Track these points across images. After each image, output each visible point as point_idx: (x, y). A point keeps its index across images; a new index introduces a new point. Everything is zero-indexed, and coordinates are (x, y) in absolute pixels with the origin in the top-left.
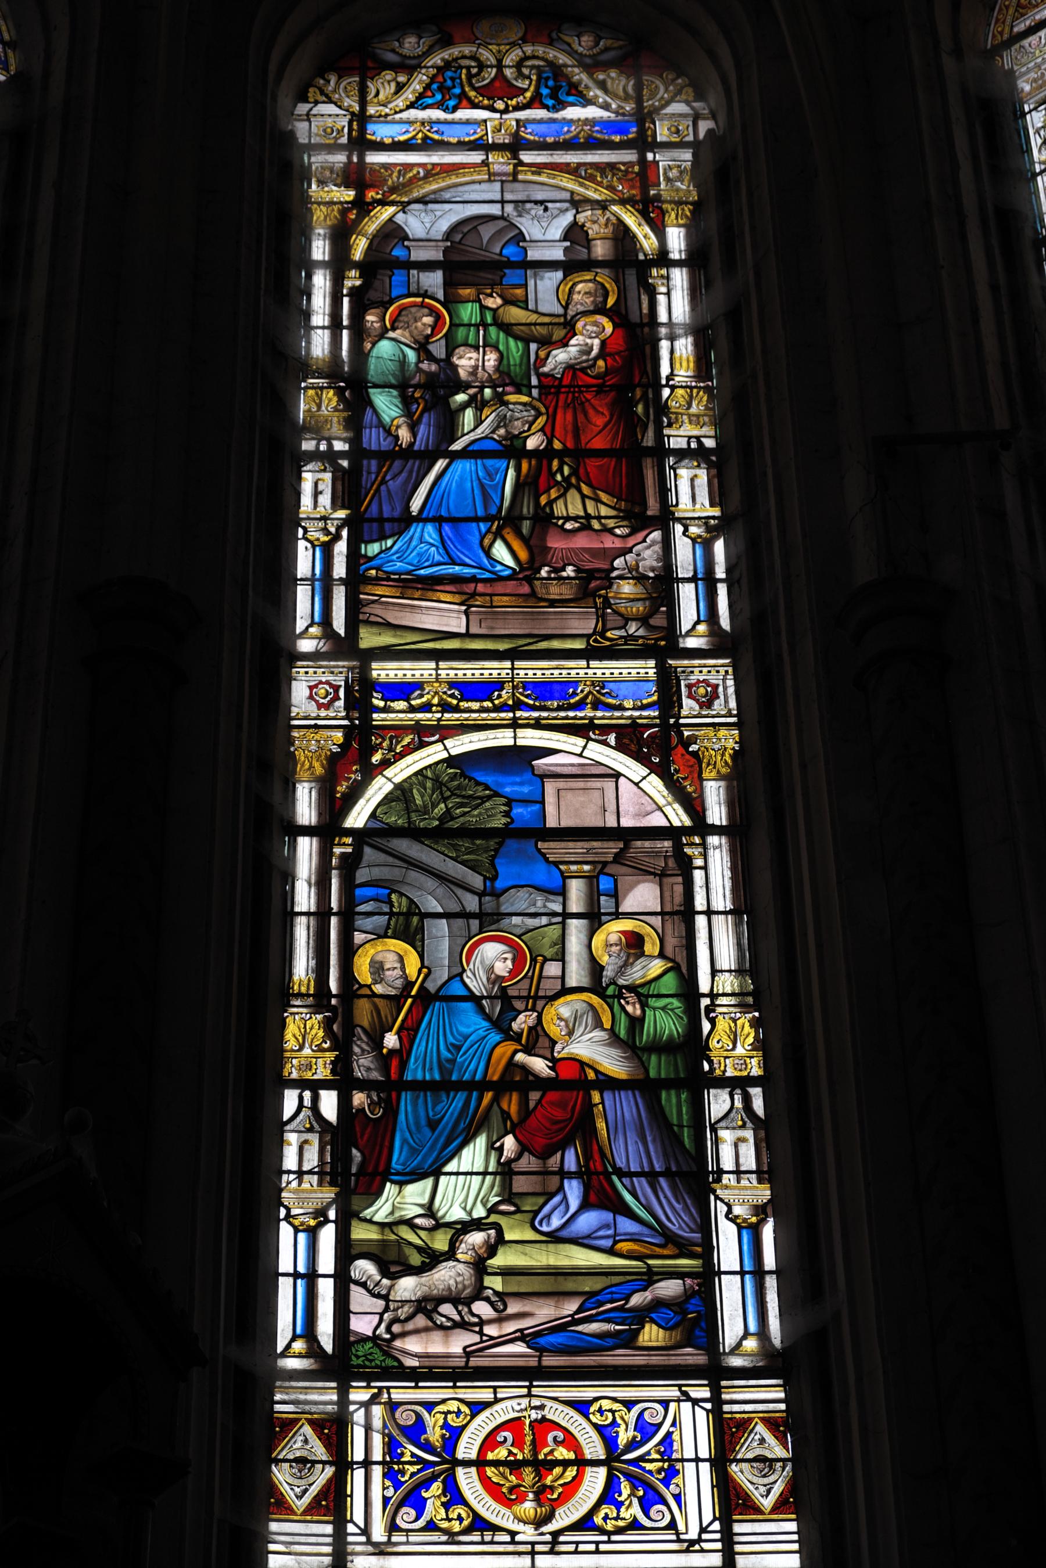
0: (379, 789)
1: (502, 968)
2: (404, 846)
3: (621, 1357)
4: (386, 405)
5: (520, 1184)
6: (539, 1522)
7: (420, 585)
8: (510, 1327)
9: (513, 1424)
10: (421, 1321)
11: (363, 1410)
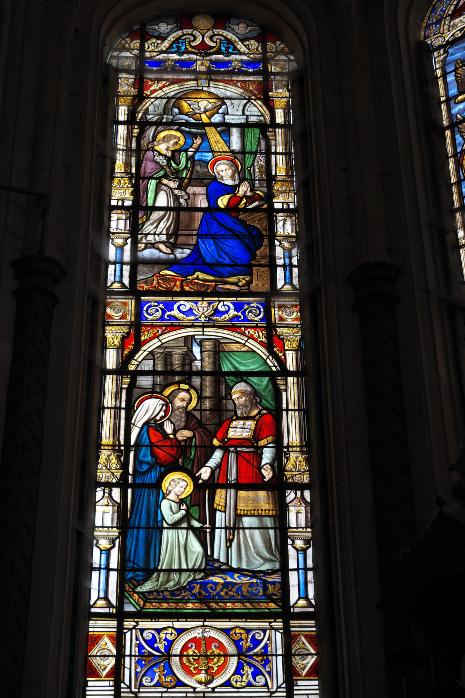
6: (206, 684)
11: (130, 632)
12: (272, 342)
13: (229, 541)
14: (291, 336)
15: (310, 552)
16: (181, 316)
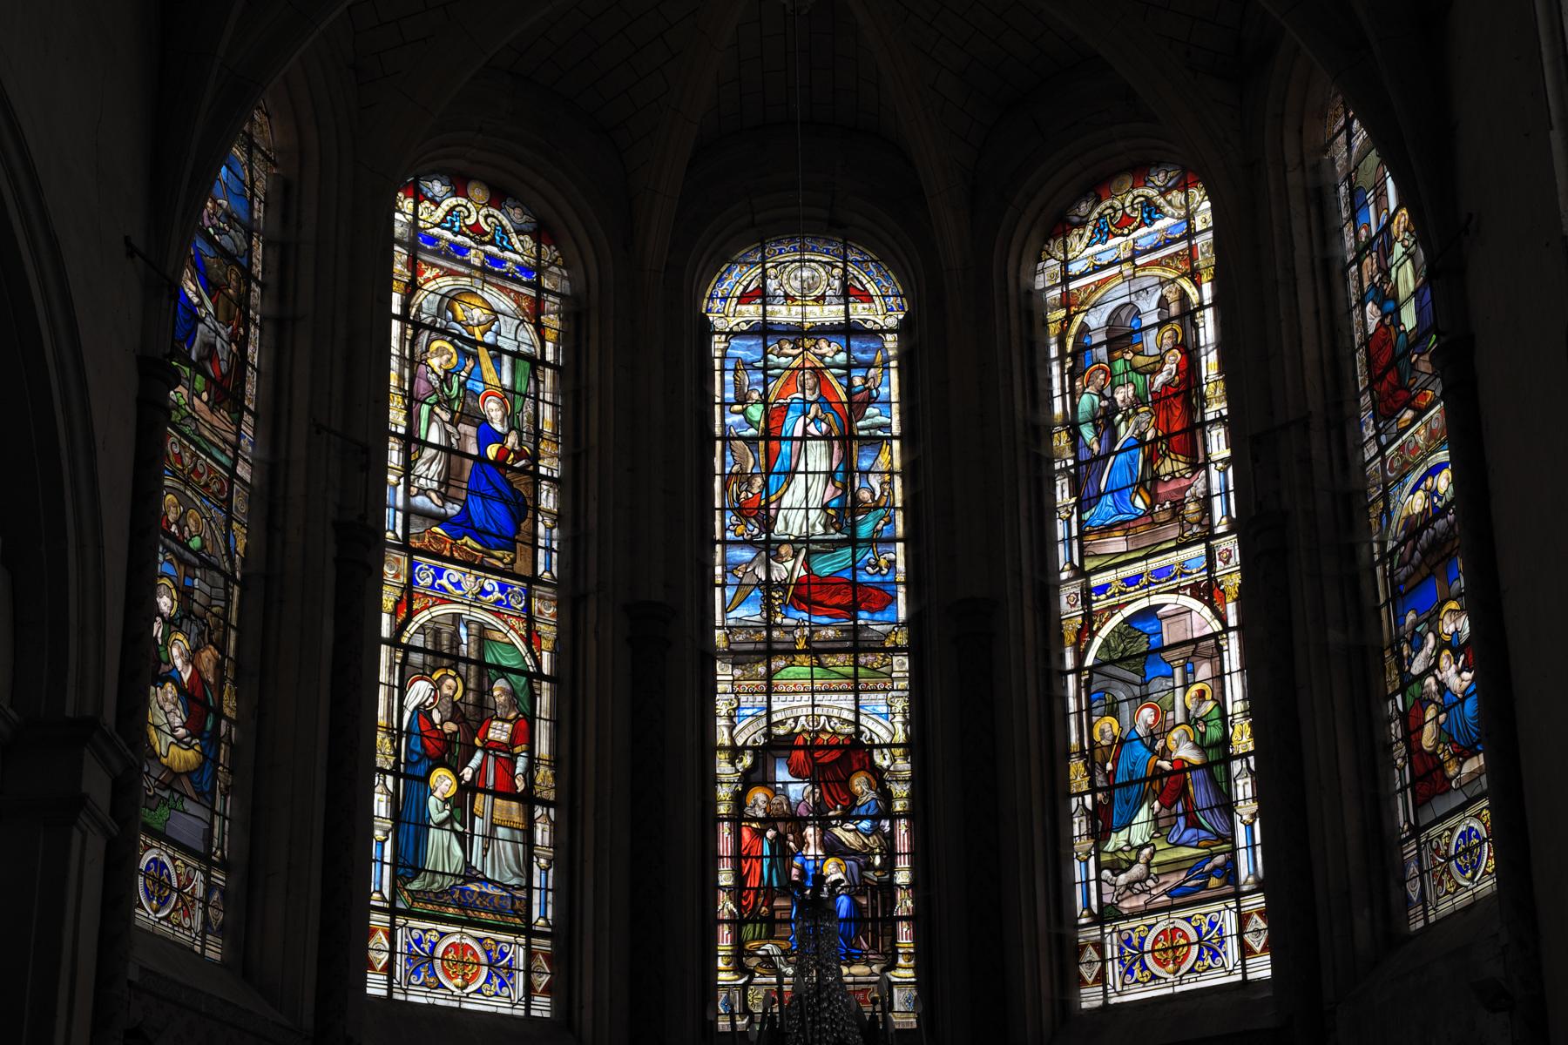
0: (1098, 642)
1: (1150, 720)
2: (1109, 669)
3: (1203, 894)
4: (1087, 432)
5: (1162, 823)
6: (463, 988)
7: (1107, 530)
8: (1161, 889)
9: (1163, 932)
10: (1128, 893)
12: (531, 638)
13: (485, 850)
14: (547, 631)
15: (551, 872)
16: (450, 587)
